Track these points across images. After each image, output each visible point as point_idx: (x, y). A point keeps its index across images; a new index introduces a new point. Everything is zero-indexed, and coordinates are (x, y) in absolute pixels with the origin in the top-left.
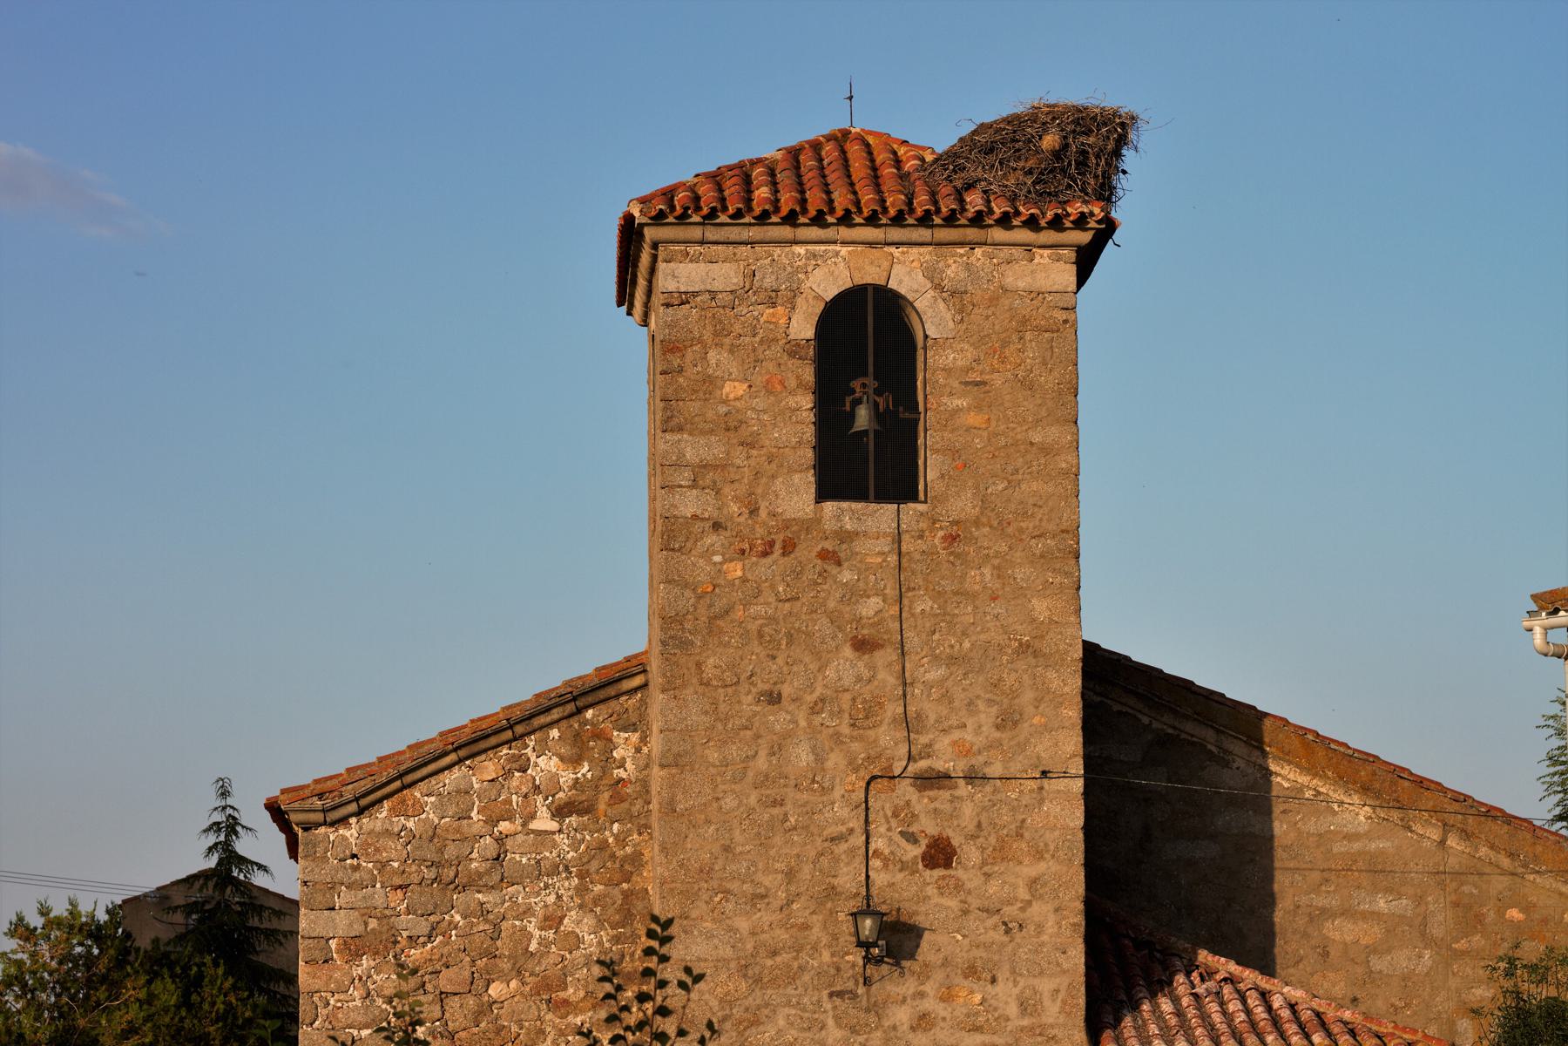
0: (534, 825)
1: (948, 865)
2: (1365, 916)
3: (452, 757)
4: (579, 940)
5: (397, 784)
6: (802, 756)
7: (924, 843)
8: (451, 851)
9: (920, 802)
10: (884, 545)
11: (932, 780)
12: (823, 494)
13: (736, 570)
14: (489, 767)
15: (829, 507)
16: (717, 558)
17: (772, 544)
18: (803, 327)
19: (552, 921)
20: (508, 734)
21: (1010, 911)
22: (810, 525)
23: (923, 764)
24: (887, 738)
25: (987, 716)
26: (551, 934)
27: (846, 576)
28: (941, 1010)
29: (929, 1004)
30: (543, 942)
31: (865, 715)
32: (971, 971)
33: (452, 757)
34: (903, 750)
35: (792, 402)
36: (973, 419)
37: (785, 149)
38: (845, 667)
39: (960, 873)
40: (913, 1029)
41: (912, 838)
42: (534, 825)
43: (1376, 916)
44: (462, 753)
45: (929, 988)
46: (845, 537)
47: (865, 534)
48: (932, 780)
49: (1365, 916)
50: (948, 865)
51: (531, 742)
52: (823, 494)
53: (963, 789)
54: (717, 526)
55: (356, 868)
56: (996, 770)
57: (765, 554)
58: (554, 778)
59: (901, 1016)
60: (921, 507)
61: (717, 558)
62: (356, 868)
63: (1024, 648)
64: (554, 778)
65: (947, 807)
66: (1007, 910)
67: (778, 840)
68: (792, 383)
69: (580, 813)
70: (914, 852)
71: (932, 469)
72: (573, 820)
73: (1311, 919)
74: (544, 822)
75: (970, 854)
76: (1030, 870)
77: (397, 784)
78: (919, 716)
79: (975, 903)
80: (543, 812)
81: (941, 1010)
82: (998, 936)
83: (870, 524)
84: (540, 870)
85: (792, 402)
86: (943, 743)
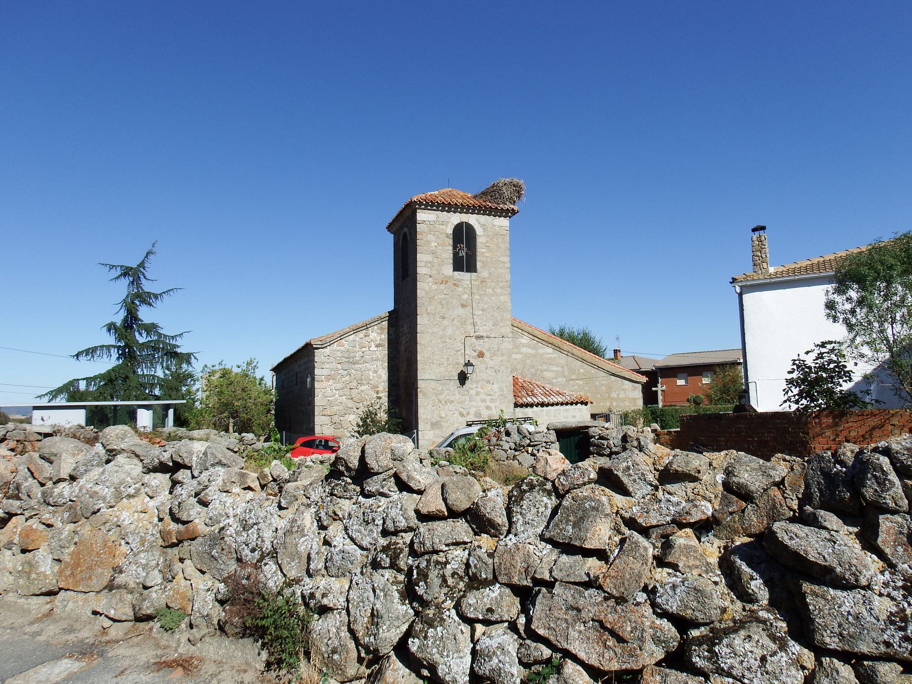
0: (371, 349)
1: (483, 357)
2: (552, 371)
3: (352, 332)
4: (382, 376)
5: (339, 338)
6: (449, 331)
7: (477, 352)
8: (352, 355)
9: (477, 342)
10: (468, 282)
11: (479, 337)
12: (454, 270)
13: (434, 287)
14: (361, 334)
15: (456, 273)
16: (431, 284)
17: (443, 281)
18: (450, 231)
19: (375, 372)
20: (366, 327)
21: (497, 368)
22: (451, 277)
23: (477, 334)
24: (470, 328)
25: (491, 323)
26: (375, 375)
27: (460, 289)
28: (482, 391)
29: (479, 389)
30: (373, 377)
31: (463, 323)
32: (488, 382)
33: (352, 332)
34: (473, 330)
35: (447, 248)
36: (487, 254)
37: (106, 325)
38: (461, 311)
39: (485, 359)
40: (476, 395)
41: (475, 351)
42: (371, 349)
43: (554, 371)
44: (355, 331)
45: (479, 386)
46: (459, 280)
47: (463, 280)
48: (479, 337)
49: (552, 371)
50: (483, 357)
51: (370, 329)
52: (454, 270)
53: (486, 339)
54: (430, 276)
55: (328, 359)
56: (492, 336)
57: (441, 284)
58: (375, 338)
59: (473, 392)
60: (476, 274)
61: (431, 284)
62: (328, 359)
63: (498, 308)
64: (375, 338)
65: (482, 343)
66: (496, 368)
67: (445, 351)
68: (447, 244)
69: (382, 346)
70: (475, 354)
71: (479, 265)
72: (380, 348)
73: (541, 371)
74: (373, 348)
75: (487, 355)
76: (500, 358)
77: (339, 338)
78: (476, 323)
79: (489, 366)
80: (373, 346)
81: (482, 391)
82: (494, 374)
83: (464, 278)
84: (373, 360)
85: (447, 248)
86: (481, 329)
